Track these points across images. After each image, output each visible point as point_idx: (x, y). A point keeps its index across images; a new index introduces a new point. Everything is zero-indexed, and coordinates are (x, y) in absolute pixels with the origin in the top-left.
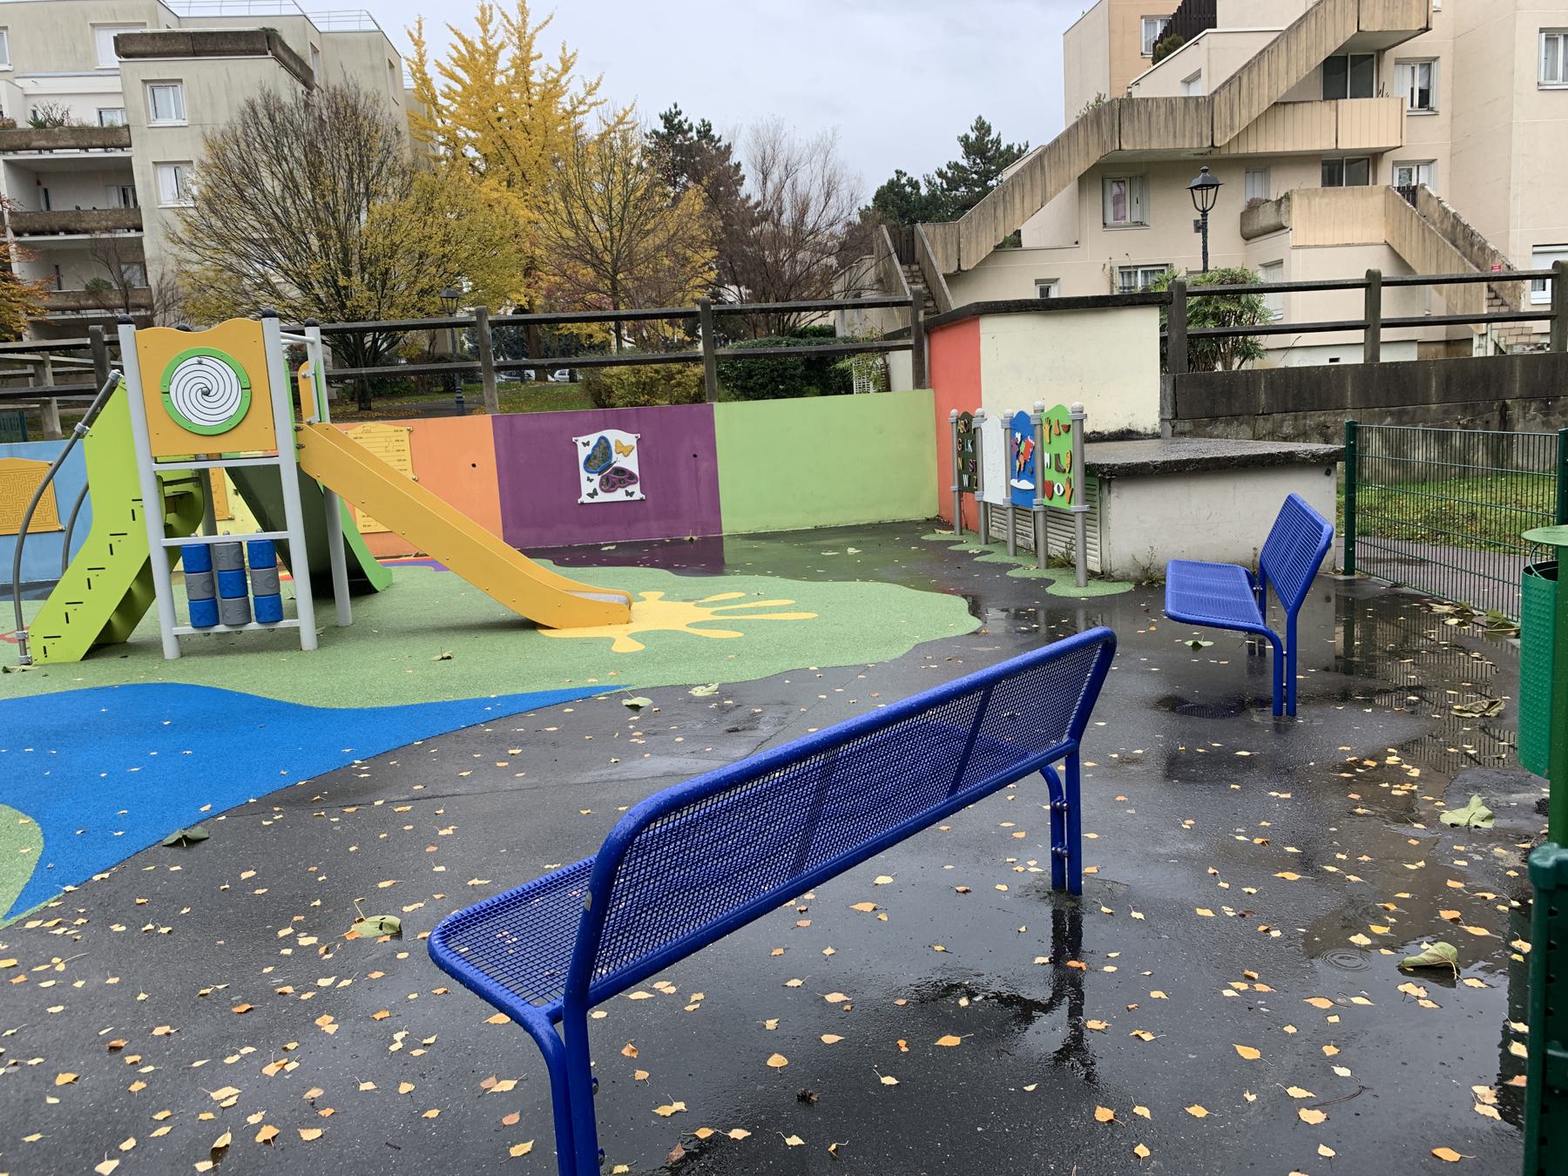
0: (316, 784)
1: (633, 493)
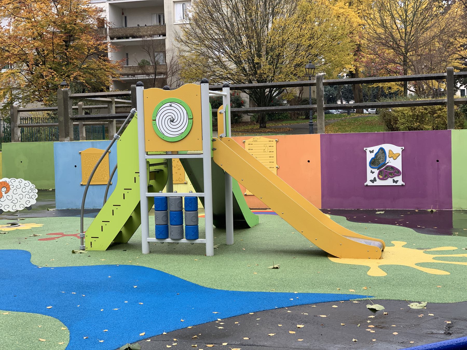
0: (197, 329)
1: (397, 181)
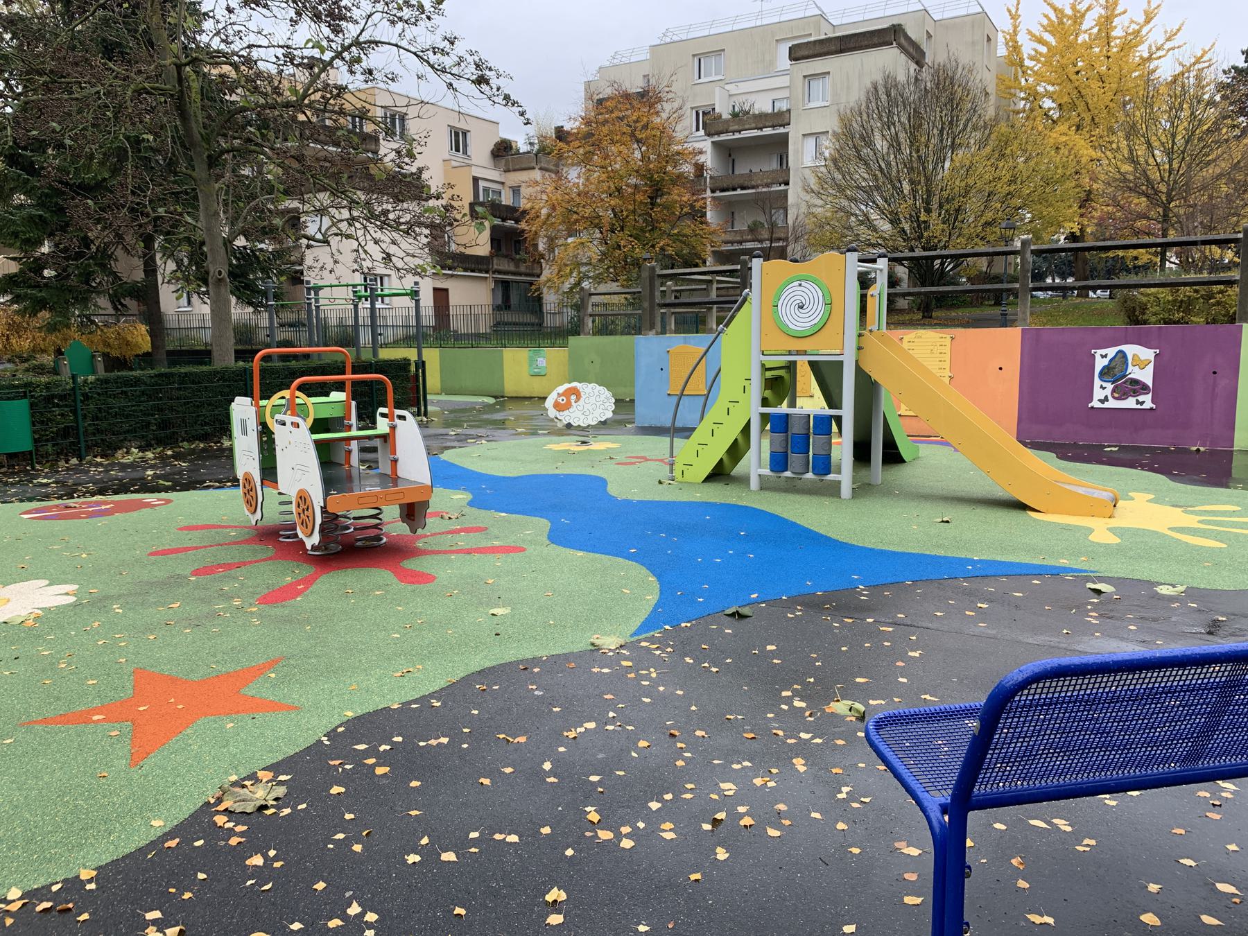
0: (829, 596)
1: (1144, 402)
